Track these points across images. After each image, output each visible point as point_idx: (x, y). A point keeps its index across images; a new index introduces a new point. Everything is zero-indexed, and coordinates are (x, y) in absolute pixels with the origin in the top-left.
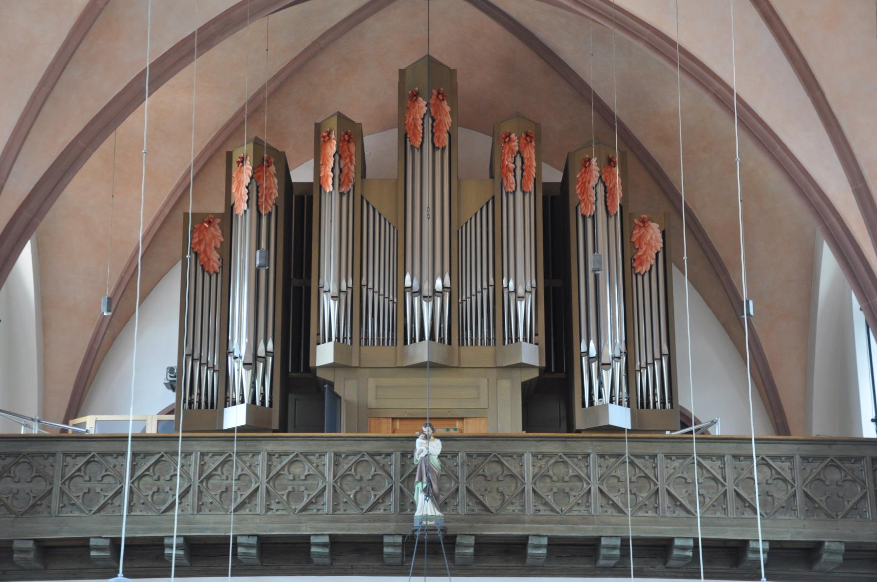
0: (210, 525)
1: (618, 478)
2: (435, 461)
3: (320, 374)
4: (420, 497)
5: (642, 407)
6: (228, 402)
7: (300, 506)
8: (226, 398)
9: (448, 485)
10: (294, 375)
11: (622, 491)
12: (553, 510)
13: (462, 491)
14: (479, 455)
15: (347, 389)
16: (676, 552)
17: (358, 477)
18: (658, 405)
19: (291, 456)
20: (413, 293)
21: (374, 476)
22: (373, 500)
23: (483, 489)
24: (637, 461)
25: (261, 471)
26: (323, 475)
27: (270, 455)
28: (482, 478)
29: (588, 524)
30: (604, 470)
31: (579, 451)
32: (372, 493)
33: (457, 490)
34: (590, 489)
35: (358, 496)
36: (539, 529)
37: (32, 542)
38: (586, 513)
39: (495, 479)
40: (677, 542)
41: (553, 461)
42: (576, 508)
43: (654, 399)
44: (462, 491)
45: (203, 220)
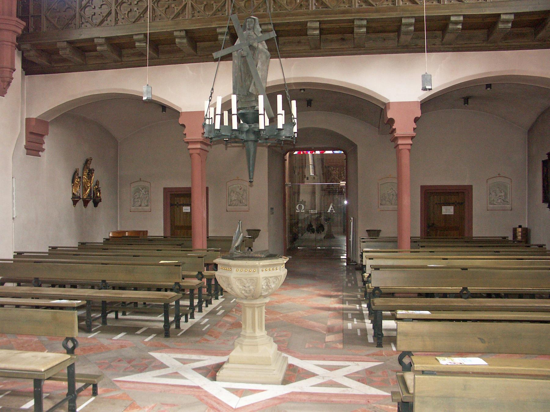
0: (164, 26)
7: (211, 13)
16: (451, 26)
26: (47, 19)
37: (65, 43)
38: (392, 5)
40: (453, 19)
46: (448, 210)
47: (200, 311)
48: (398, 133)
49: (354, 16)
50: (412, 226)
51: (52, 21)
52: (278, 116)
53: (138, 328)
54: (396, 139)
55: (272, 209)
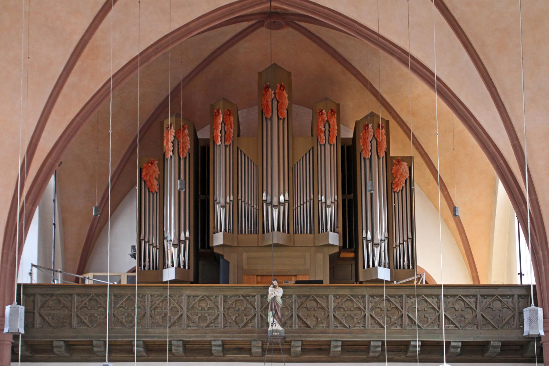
1: (381, 308)
2: (279, 301)
3: (215, 250)
4: (271, 319)
5: (397, 268)
6: (164, 266)
7: (205, 325)
8: (164, 264)
9: (287, 313)
10: (203, 250)
11: (383, 316)
12: (345, 326)
13: (295, 316)
14: (304, 296)
15: (231, 258)
17: (237, 309)
18: (406, 267)
19: (200, 297)
20: (267, 204)
21: (245, 308)
22: (245, 321)
23: (306, 315)
25: (184, 305)
27: (189, 296)
28: (306, 309)
29: (364, 334)
30: (373, 304)
31: (359, 294)
32: (245, 317)
33: (292, 316)
34: (365, 315)
35: (237, 319)
36: (336, 338)
38: (363, 328)
39: (313, 309)
41: (345, 299)
42: (357, 325)
43: (403, 264)
44: (295, 316)
49: (332, 337)
51: (46, 318)
52: (523, 283)
53: (115, 85)
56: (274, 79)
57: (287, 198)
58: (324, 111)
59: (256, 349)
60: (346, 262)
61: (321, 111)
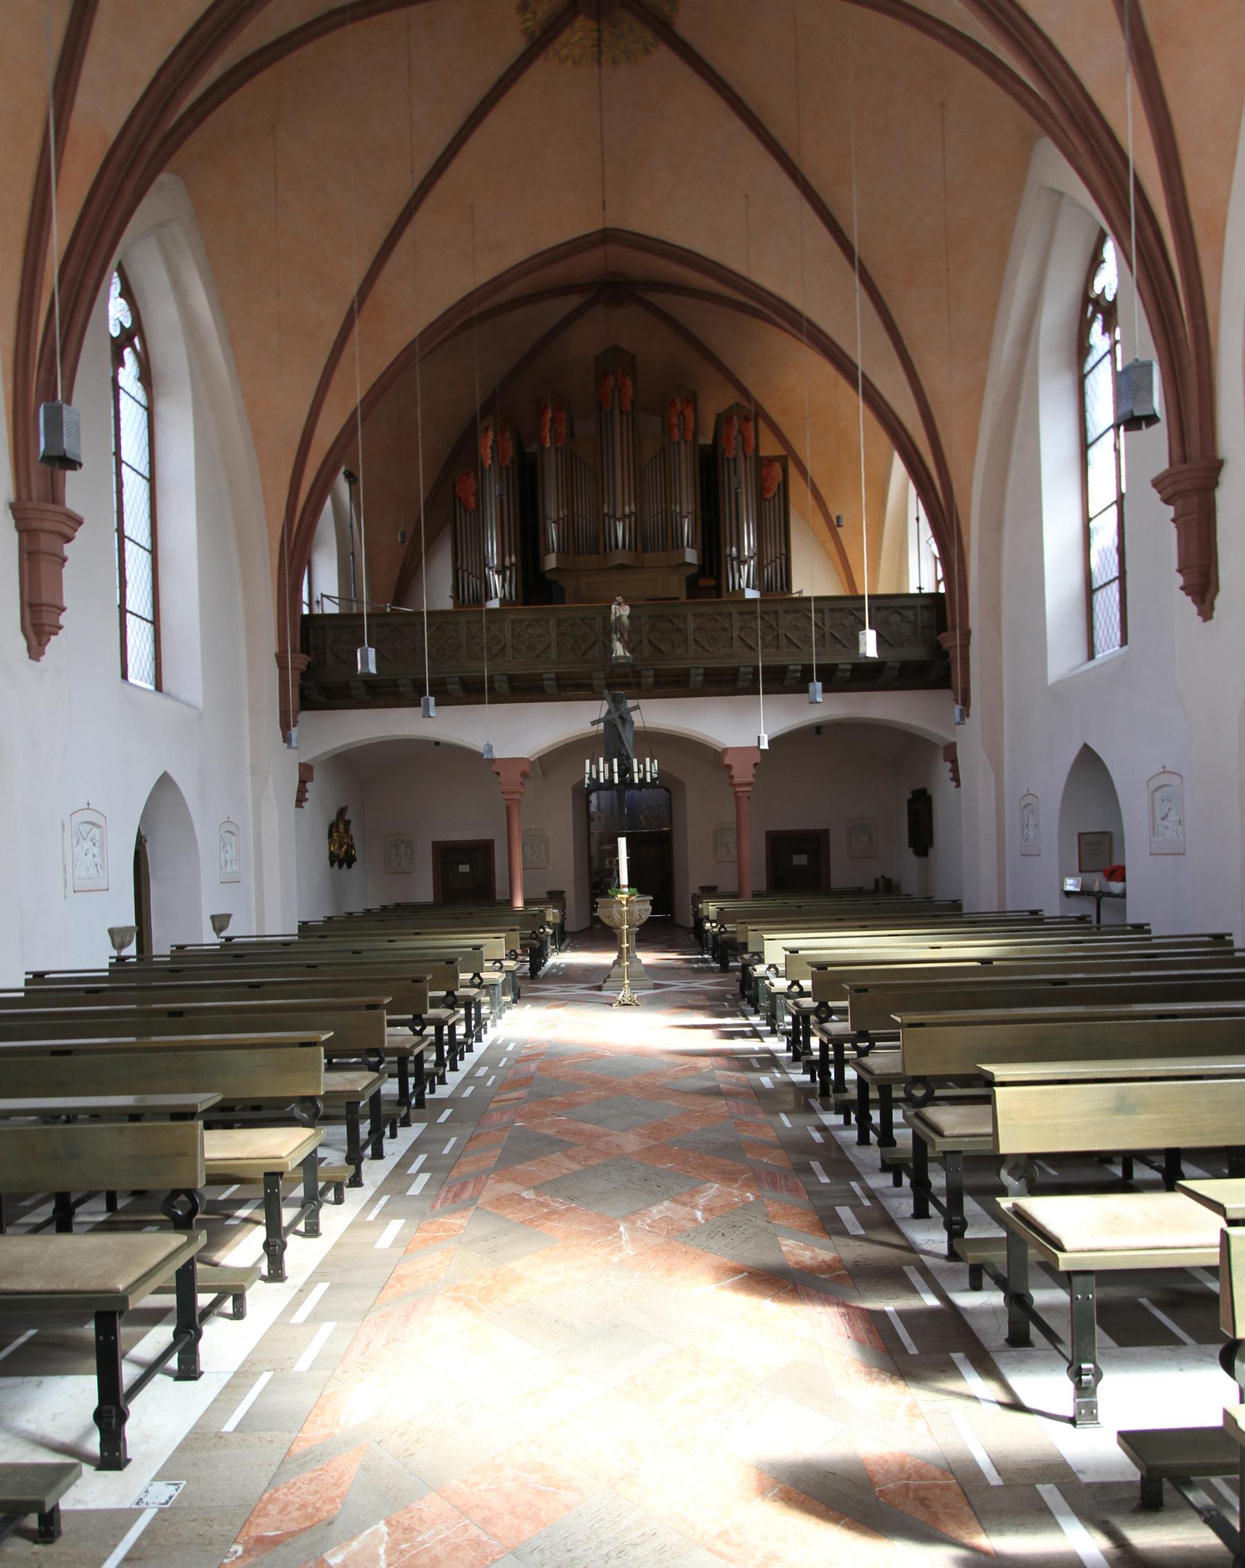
2: (625, 620)
3: (547, 576)
16: (789, 675)
20: (610, 517)
24: (766, 617)
27: (513, 622)
33: (641, 641)
45: (558, 686)
46: (800, 860)
47: (378, 1154)
48: (736, 780)
50: (757, 877)
54: (734, 785)
55: (839, 526)
56: (615, 362)
57: (633, 510)
58: (677, 401)
59: (599, 680)
60: (711, 574)
61: (674, 400)
